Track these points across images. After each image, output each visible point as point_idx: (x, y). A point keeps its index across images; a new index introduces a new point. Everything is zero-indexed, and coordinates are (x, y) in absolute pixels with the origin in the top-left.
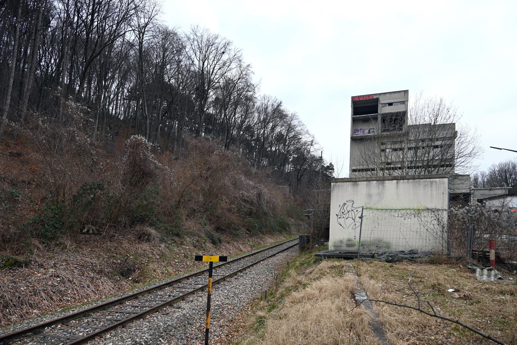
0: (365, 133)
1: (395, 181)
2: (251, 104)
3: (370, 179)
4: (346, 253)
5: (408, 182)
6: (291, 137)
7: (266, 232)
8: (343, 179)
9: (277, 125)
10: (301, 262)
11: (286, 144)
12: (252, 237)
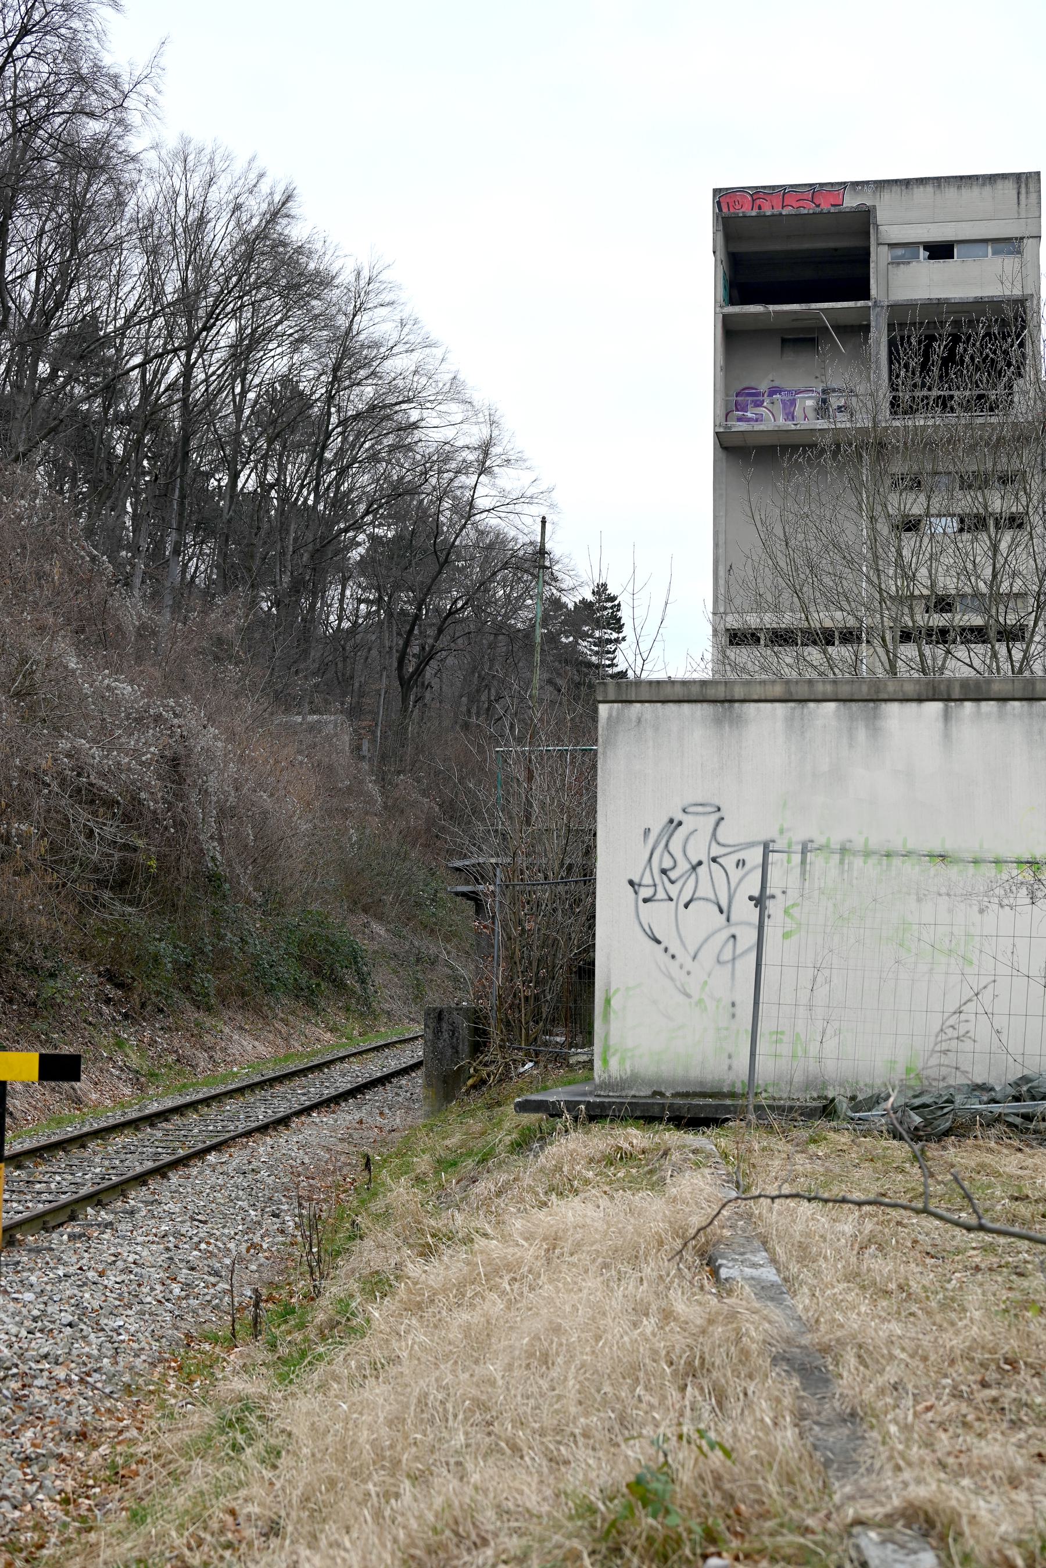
0: (798, 411)
1: (934, 708)
2: (102, 192)
3: (803, 691)
4: (687, 1095)
5: (1001, 717)
6: (358, 416)
7: (223, 996)
8: (658, 683)
9: (268, 334)
10: (441, 1152)
11: (328, 455)
12: (135, 1022)
